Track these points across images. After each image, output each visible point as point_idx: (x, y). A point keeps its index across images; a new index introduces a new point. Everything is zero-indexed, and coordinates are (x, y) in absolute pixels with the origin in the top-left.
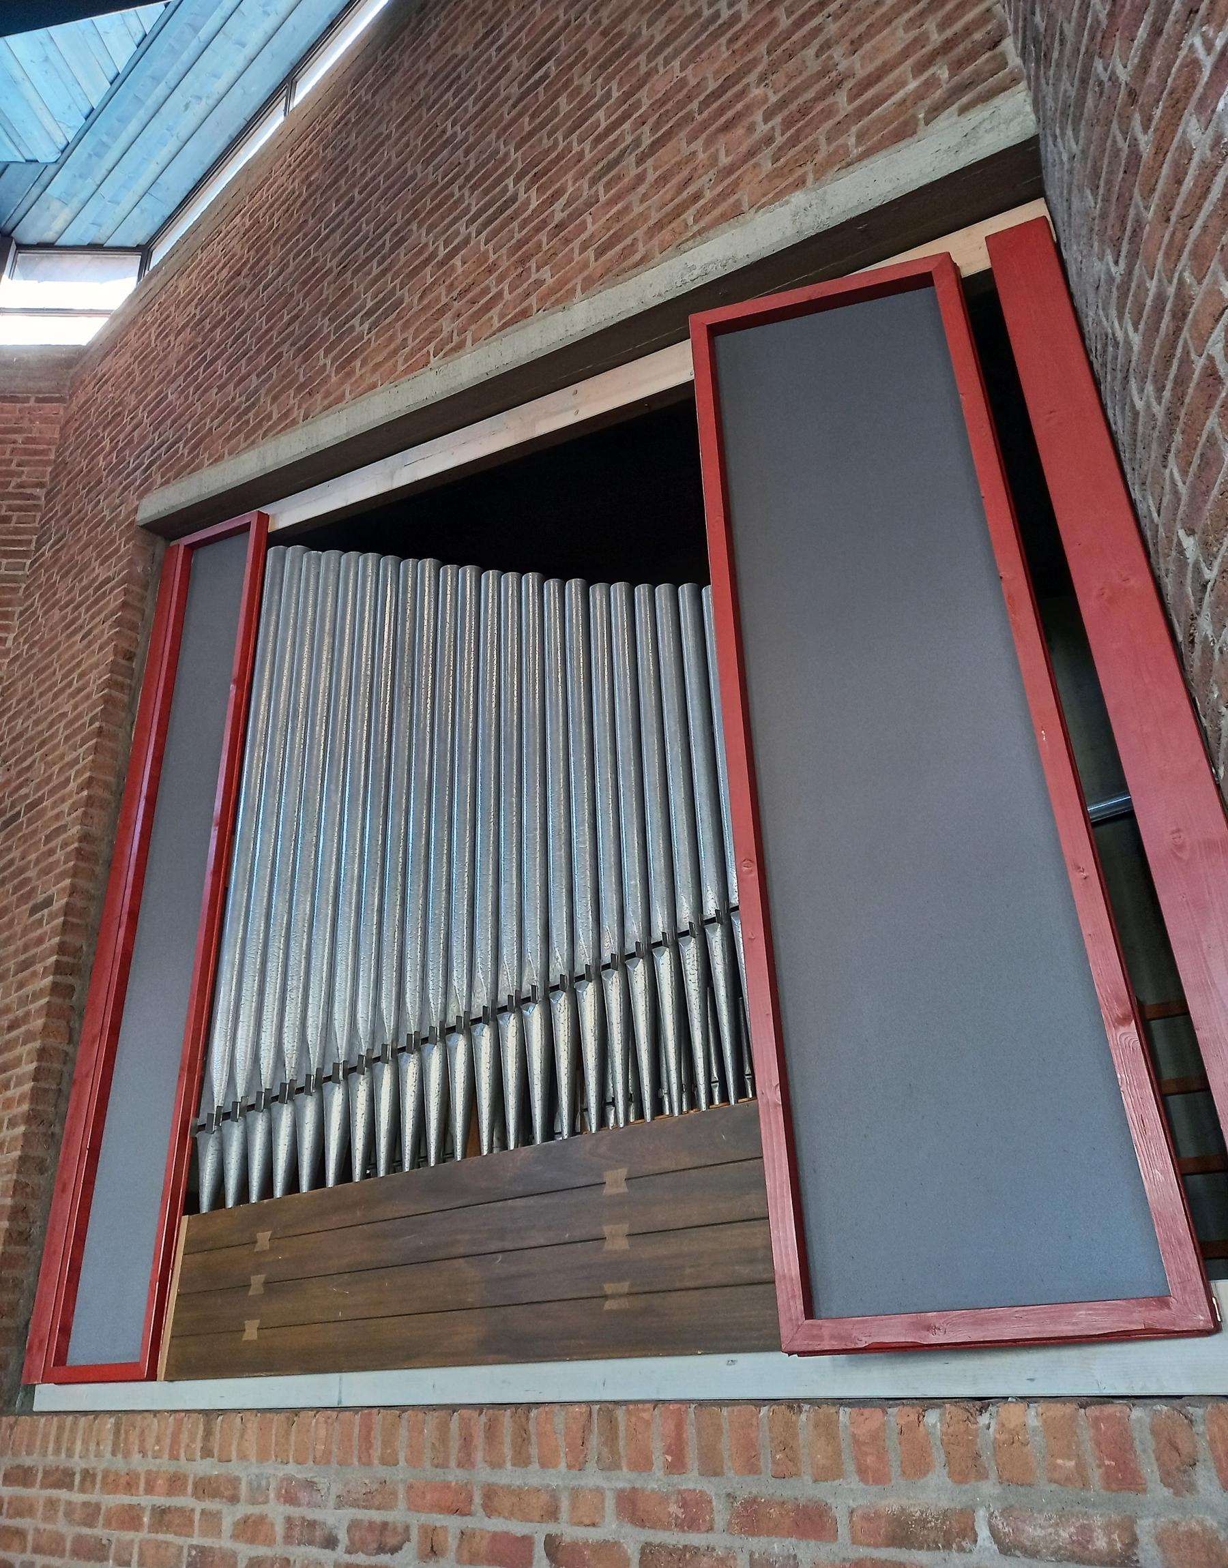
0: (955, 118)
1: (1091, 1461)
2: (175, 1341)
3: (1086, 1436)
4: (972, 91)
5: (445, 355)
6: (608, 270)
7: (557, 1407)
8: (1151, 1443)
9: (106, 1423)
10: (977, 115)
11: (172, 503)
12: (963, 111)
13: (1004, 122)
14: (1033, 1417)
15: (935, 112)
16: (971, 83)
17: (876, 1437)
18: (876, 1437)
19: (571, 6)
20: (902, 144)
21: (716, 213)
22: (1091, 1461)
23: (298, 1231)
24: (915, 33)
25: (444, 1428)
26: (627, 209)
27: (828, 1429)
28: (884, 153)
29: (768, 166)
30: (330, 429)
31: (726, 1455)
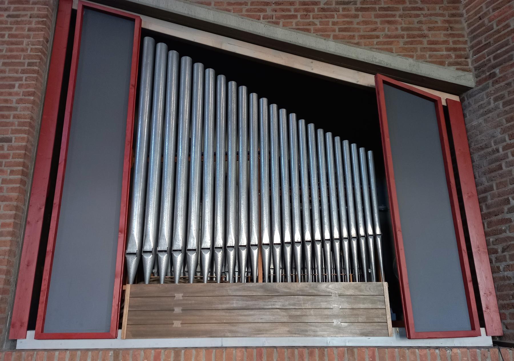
0: (455, 69)
1: (469, 358)
2: (128, 326)
3: (469, 354)
4: (459, 65)
5: (269, 22)
6: (344, 38)
7: (334, 349)
8: (480, 355)
9: (109, 353)
10: (460, 73)
11: (231, 24)
12: (457, 69)
13: (467, 80)
14: (458, 351)
15: (450, 64)
16: (460, 64)
17: (425, 355)
18: (425, 355)
19: (490, 3)
20: (440, 66)
21: (385, 47)
22: (469, 358)
23: (197, 295)
24: (445, 39)
25: (293, 354)
26: (351, 23)
27: (414, 353)
28: (436, 65)
29: (401, 45)
30: (280, 34)
31: (387, 358)
